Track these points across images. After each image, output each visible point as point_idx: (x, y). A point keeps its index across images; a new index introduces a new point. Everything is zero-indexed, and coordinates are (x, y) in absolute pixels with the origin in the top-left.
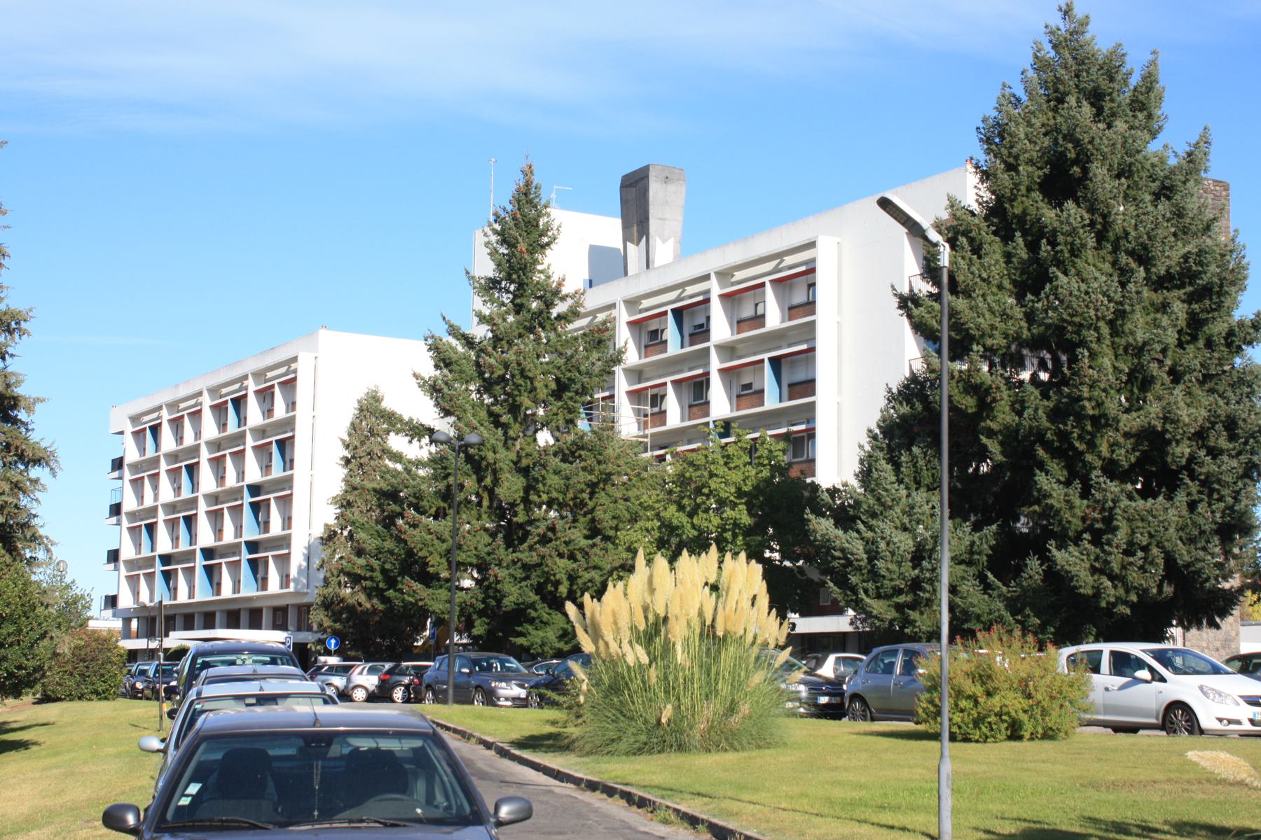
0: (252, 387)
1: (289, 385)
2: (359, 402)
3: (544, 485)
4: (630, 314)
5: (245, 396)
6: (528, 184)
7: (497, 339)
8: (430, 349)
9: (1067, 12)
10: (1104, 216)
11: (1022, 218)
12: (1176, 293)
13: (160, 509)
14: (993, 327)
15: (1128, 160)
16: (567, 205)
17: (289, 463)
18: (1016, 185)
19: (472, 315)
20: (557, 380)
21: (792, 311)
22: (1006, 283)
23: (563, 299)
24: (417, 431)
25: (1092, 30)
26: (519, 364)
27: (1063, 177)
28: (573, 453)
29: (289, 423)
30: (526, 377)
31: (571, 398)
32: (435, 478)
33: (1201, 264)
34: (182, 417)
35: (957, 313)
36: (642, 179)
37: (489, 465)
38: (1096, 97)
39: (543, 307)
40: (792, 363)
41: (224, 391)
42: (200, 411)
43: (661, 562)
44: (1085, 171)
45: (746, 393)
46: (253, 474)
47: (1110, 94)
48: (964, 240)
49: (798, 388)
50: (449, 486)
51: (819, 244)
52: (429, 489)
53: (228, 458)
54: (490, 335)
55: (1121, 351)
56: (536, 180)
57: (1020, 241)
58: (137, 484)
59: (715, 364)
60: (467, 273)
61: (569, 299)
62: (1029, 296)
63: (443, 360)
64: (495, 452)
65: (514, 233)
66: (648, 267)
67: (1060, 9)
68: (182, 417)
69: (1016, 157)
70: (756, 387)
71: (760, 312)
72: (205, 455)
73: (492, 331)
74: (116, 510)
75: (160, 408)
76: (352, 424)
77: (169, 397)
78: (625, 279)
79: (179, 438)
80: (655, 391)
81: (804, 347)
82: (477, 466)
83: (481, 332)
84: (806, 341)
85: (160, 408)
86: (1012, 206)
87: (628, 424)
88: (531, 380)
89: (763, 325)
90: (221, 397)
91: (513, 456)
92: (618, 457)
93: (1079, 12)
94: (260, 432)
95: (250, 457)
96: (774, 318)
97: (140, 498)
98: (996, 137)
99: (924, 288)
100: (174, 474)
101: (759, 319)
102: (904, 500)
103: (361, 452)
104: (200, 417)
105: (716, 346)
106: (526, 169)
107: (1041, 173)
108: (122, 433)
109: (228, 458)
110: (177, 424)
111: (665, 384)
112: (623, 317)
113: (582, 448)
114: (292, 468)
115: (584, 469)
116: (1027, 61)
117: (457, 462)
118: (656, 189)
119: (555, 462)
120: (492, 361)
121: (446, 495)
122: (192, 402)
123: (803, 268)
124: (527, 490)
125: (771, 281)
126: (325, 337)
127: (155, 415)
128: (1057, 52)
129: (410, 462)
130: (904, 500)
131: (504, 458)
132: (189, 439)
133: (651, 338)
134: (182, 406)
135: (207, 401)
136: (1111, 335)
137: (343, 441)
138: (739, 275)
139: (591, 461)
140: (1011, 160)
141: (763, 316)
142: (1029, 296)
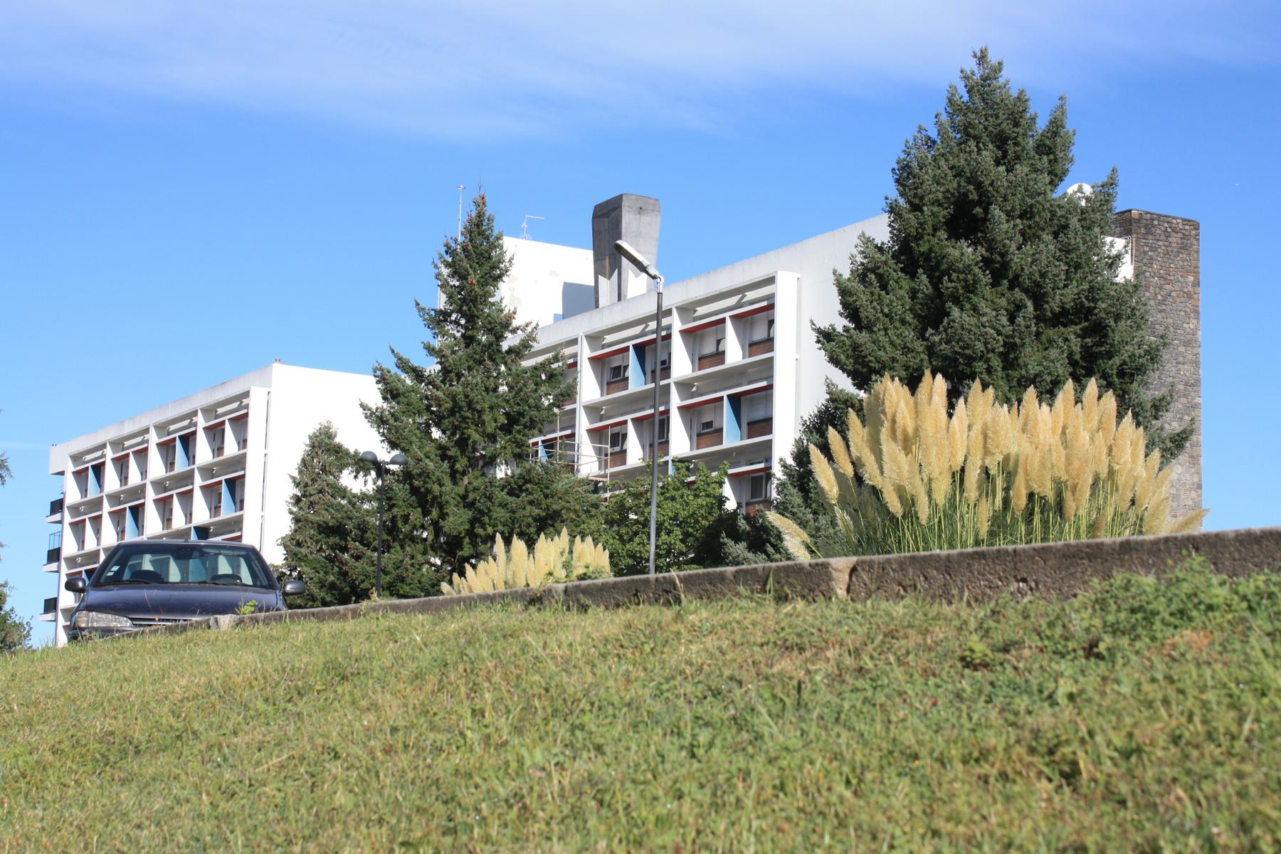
0: (201, 422)
1: (240, 422)
2: (310, 438)
3: (490, 518)
4: (592, 350)
5: (194, 433)
6: (480, 215)
7: (445, 371)
8: (378, 382)
9: (982, 58)
10: (1002, 255)
11: (927, 256)
12: (1072, 328)
13: (105, 501)
14: (894, 360)
15: (1029, 201)
16: (516, 234)
17: (239, 503)
18: (921, 225)
19: (418, 346)
20: (507, 414)
21: (753, 347)
22: (909, 317)
23: (514, 331)
24: (365, 463)
25: (1005, 75)
26: (467, 396)
27: (966, 218)
28: (520, 487)
29: (240, 462)
30: (474, 410)
31: (519, 432)
32: (380, 510)
33: (1094, 300)
34: (128, 455)
35: (861, 346)
36: (615, 209)
37: (435, 498)
38: (1001, 141)
39: (492, 339)
40: (752, 400)
41: (172, 428)
42: (146, 449)
43: (519, 545)
44: (986, 211)
45: (705, 431)
46: (201, 514)
47: (1015, 138)
48: (873, 276)
49: (757, 426)
50: (393, 519)
51: (779, 280)
52: (374, 521)
53: (175, 500)
54: (439, 367)
55: (1014, 383)
56: (489, 211)
57: (924, 277)
58: (78, 527)
59: (676, 400)
60: (417, 304)
61: (519, 332)
62: (930, 331)
63: (391, 393)
64: (441, 485)
65: (465, 264)
66: (619, 299)
67: (975, 56)
68: (128, 455)
69: (922, 198)
70: (716, 426)
71: (721, 349)
72: (151, 495)
73: (440, 363)
74: (54, 555)
75: (103, 446)
76: (303, 460)
77: (112, 434)
78: (595, 312)
79: (124, 478)
80: (616, 429)
81: (764, 384)
82: (424, 500)
83: (432, 367)
84: (766, 379)
85: (103, 446)
86: (918, 245)
87: (588, 464)
88: (480, 412)
89: (723, 362)
90: (169, 434)
91: (461, 490)
92: (567, 492)
93: (993, 58)
94: (207, 471)
95: (198, 497)
96: (734, 354)
97: (81, 542)
98: (905, 175)
99: (841, 323)
100: (117, 517)
101: (719, 356)
102: (811, 522)
103: (311, 490)
104: (146, 456)
105: (676, 383)
106: (479, 200)
107: (945, 212)
108: (62, 473)
109: (175, 500)
110: (121, 463)
111: (625, 422)
112: (585, 352)
113: (530, 481)
114: (242, 509)
115: (531, 503)
116: (941, 105)
117: (401, 491)
118: (628, 219)
119: (502, 496)
120: (440, 394)
121: (392, 529)
122: (139, 439)
123: (765, 304)
124: (473, 522)
125: (731, 317)
126: (279, 371)
127: (99, 454)
128: (970, 97)
129: (355, 496)
130: (811, 522)
131: (450, 491)
132: (134, 478)
133: (611, 372)
134: (127, 444)
135: (154, 439)
136: (1004, 369)
137: (294, 479)
138: (701, 310)
139: (538, 495)
140: (917, 201)
141: (723, 353)
142: (930, 331)
